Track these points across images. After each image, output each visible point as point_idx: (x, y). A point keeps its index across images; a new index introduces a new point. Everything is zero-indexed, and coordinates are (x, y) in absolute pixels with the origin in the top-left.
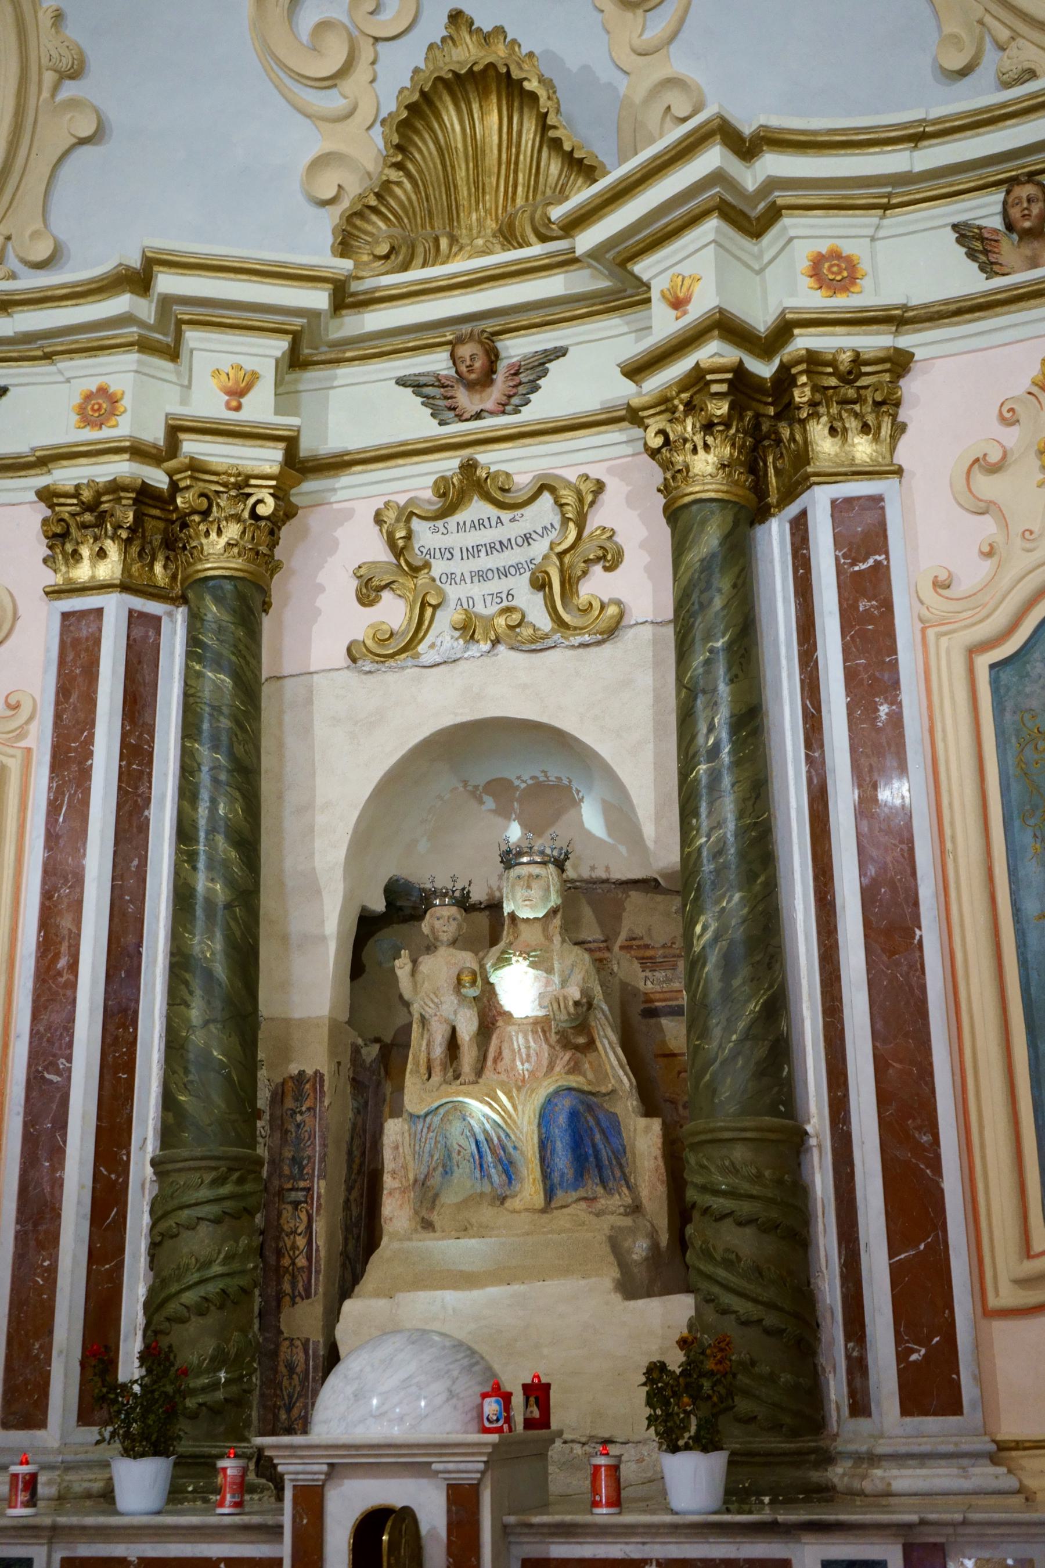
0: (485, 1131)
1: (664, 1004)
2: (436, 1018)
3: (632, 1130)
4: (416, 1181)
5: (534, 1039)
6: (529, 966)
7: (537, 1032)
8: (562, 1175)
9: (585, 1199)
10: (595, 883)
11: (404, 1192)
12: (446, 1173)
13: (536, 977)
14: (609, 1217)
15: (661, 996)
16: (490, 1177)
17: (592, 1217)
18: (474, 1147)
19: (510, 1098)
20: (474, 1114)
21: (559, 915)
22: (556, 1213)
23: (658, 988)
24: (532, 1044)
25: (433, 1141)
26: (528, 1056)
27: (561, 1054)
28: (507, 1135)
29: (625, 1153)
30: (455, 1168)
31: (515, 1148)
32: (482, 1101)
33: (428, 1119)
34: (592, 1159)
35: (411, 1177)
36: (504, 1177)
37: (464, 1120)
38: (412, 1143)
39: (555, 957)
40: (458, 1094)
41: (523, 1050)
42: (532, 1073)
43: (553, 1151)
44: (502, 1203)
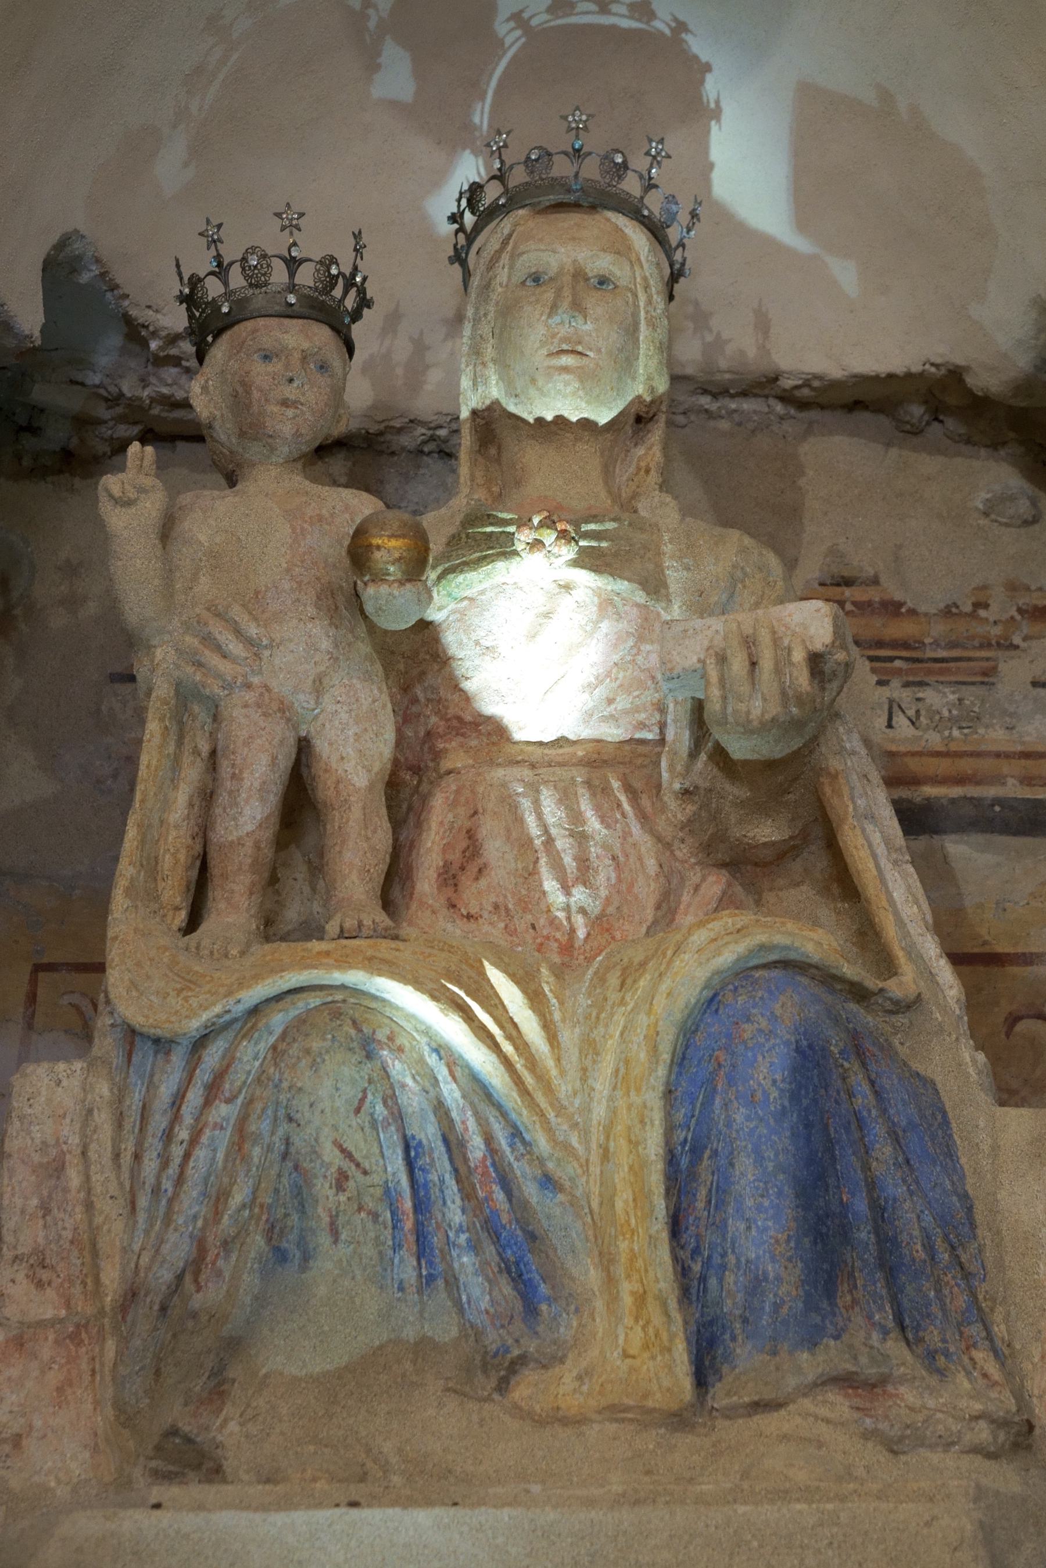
0: (440, 1108)
1: (956, 792)
2: (250, 697)
3: (985, 1147)
4: (132, 1295)
5: (597, 808)
6: (576, 563)
7: (606, 790)
8: (756, 1285)
9: (846, 1381)
10: (720, 392)
11: (75, 1337)
12: (281, 1256)
13: (606, 605)
14: (935, 1457)
15: (942, 767)
16: (452, 1283)
17: (873, 1453)
18: (397, 1164)
19: (535, 999)
20: (402, 1040)
21: (657, 434)
22: (730, 1431)
23: (934, 740)
24: (594, 824)
25: (224, 1139)
26: (584, 863)
27: (694, 877)
28: (516, 1133)
29: (973, 1226)
30: (324, 1240)
31: (548, 1182)
32: (438, 995)
33: (213, 1056)
34: (864, 1234)
35: (112, 1277)
36: (507, 1289)
37: (369, 1056)
38: (128, 1147)
39: (668, 548)
40: (344, 963)
41: (563, 843)
42: (600, 923)
43: (719, 1197)
44: (503, 1386)
